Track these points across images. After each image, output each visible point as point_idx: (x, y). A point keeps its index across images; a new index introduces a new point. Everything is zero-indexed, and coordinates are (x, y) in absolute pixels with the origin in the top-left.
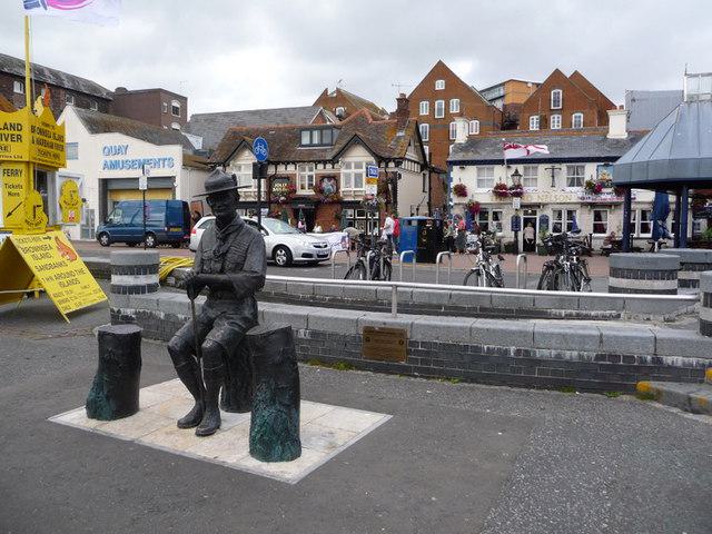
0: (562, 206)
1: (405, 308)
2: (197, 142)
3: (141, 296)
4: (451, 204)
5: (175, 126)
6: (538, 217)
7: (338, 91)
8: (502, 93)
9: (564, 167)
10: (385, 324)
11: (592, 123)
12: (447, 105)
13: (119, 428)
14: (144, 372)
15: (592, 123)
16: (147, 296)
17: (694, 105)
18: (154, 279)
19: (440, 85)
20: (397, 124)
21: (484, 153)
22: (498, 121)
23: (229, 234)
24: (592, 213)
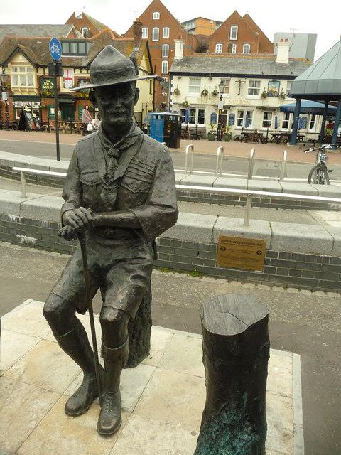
0: (245, 108)
6: (228, 115)
7: (83, 15)
9: (247, 80)
10: (243, 234)
11: (255, 51)
12: (161, 31)
19: (156, 16)
21: (194, 68)
22: (195, 47)
23: (126, 149)
24: (263, 113)
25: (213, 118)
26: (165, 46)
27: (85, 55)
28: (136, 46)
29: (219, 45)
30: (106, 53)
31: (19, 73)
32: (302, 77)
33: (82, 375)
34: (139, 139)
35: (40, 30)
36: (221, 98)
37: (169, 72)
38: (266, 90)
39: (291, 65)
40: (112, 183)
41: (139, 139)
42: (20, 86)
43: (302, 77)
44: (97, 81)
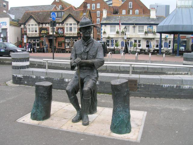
1: (50, 67)
2: (13, 17)
3: (24, 70)
4: (102, 37)
5: (5, 11)
8: (111, 2)
9: (137, 26)
10: (129, 78)
12: (96, 6)
13: (45, 123)
14: (52, 100)
15: (141, 13)
16: (27, 69)
17: (180, 9)
18: (27, 63)
20: (83, 11)
22: (112, 11)
23: (89, 44)
25: (122, 43)
26: (98, 12)
27: (61, 17)
28: (85, 13)
29: (124, 10)
30: (84, 19)
31: (31, 27)
32: (161, 24)
33: (76, 113)
34: (92, 41)
35: (40, 8)
36: (125, 34)
37: (100, 24)
38: (147, 30)
39: (157, 19)
40: (86, 53)
41: (93, 41)
42: (31, 33)
43: (161, 24)
44: (81, 26)
